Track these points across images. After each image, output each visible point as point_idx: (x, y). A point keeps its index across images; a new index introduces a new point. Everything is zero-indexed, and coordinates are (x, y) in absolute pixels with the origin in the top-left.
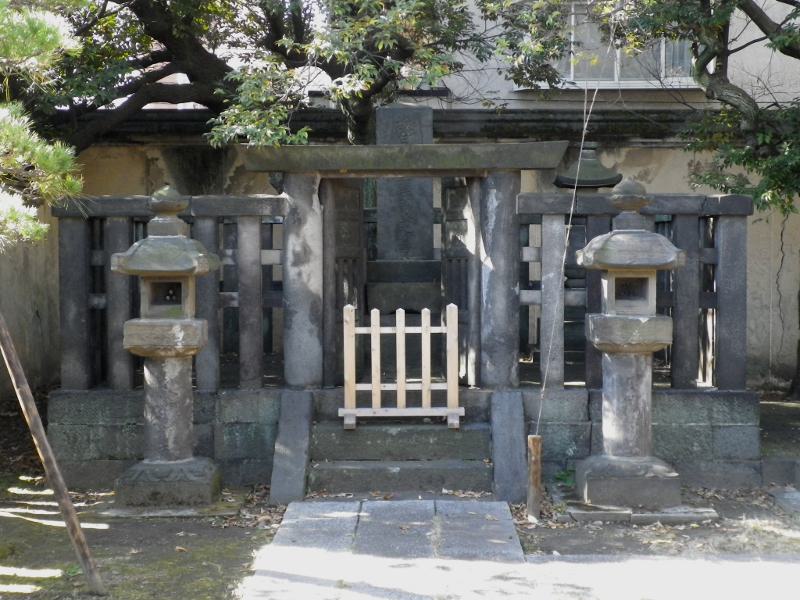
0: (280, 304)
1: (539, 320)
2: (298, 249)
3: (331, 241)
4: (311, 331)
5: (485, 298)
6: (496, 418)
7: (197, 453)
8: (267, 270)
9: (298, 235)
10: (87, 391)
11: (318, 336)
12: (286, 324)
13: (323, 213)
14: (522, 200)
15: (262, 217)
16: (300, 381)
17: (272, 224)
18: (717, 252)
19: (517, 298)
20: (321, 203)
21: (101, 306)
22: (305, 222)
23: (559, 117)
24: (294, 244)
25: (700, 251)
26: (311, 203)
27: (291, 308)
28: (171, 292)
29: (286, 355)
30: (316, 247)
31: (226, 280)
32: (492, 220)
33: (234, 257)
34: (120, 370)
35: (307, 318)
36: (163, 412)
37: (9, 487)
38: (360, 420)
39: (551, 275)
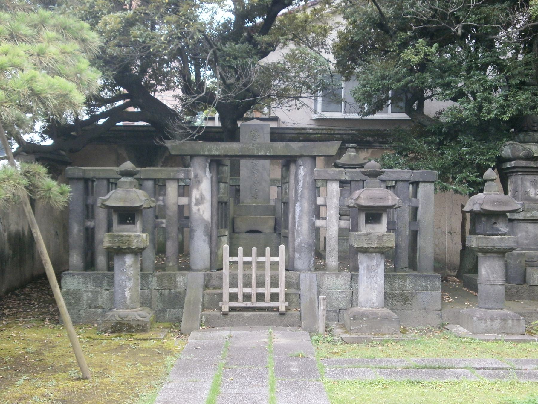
0: (188, 226)
1: (325, 238)
2: (198, 196)
3: (215, 213)
4: (204, 240)
5: (297, 224)
6: (302, 287)
7: (143, 304)
8: (181, 208)
9: (198, 189)
10: (83, 272)
11: (208, 243)
12: (191, 237)
13: (212, 178)
14: (316, 172)
15: (178, 180)
16: (199, 267)
17: (184, 185)
18: (418, 200)
19: (314, 224)
20: (210, 172)
21: (92, 226)
22: (202, 183)
23: (336, 132)
24: (195, 194)
25: (410, 200)
26: (205, 172)
27: (194, 228)
28: (129, 218)
29: (190, 253)
30: (207, 195)
31: (160, 212)
32: (301, 184)
33: (163, 201)
34: (101, 260)
35: (202, 233)
36: (124, 283)
37: (127, 94)
38: (232, 309)
39: (332, 212)
